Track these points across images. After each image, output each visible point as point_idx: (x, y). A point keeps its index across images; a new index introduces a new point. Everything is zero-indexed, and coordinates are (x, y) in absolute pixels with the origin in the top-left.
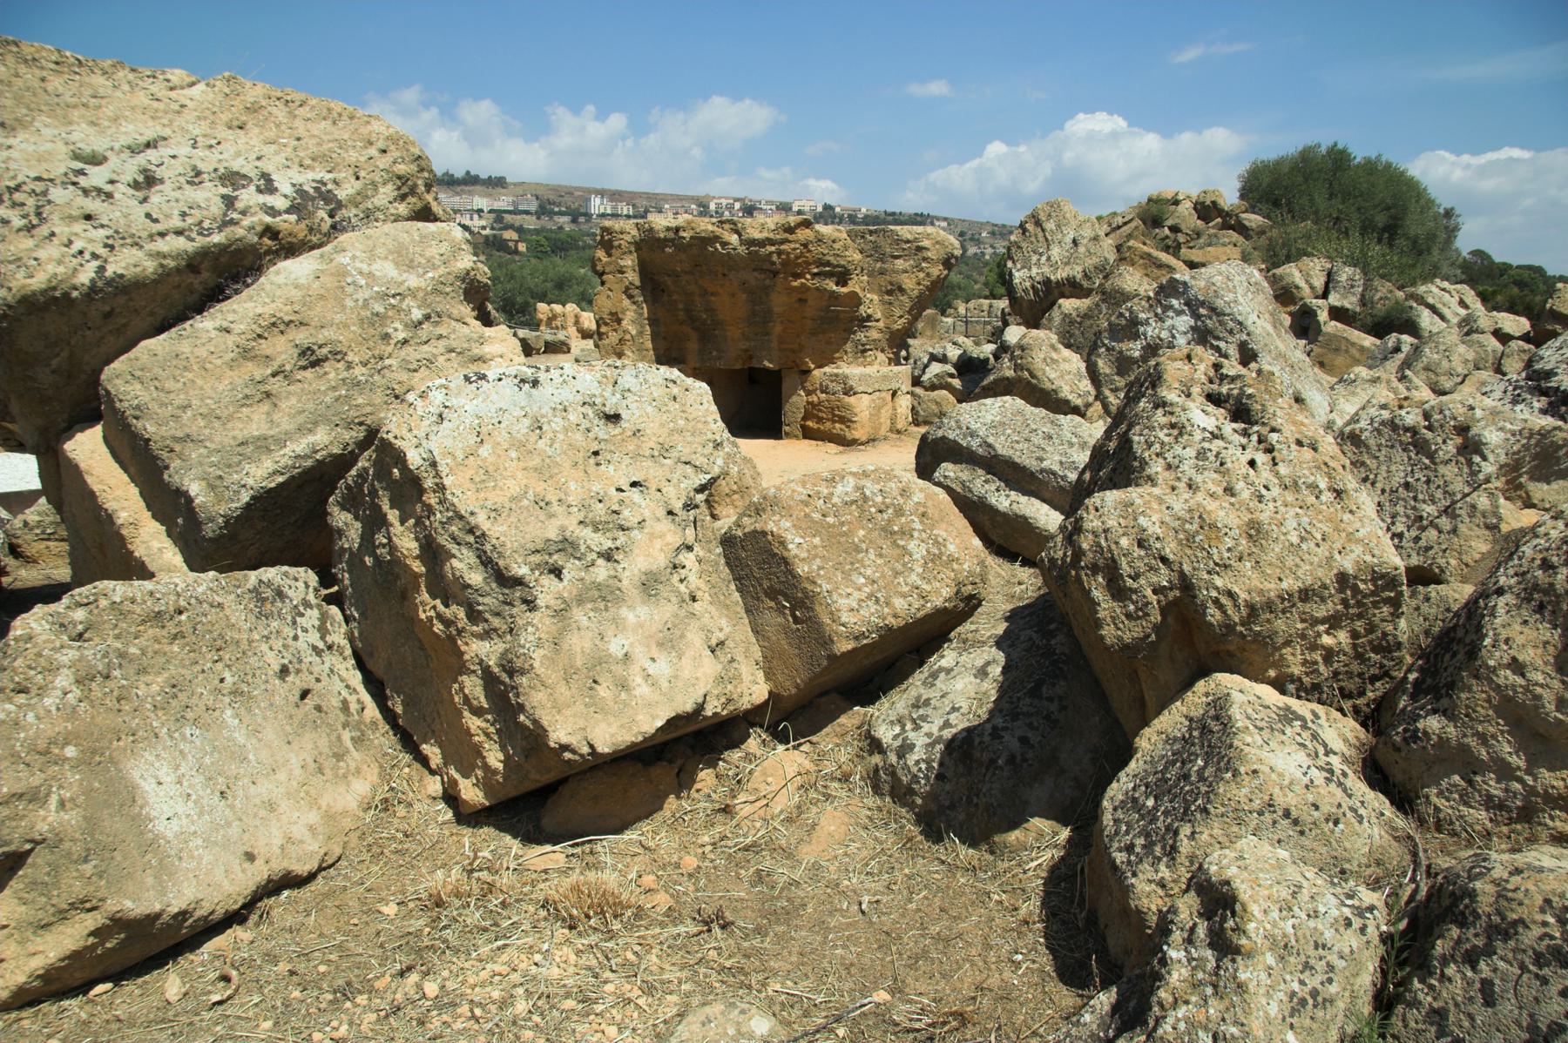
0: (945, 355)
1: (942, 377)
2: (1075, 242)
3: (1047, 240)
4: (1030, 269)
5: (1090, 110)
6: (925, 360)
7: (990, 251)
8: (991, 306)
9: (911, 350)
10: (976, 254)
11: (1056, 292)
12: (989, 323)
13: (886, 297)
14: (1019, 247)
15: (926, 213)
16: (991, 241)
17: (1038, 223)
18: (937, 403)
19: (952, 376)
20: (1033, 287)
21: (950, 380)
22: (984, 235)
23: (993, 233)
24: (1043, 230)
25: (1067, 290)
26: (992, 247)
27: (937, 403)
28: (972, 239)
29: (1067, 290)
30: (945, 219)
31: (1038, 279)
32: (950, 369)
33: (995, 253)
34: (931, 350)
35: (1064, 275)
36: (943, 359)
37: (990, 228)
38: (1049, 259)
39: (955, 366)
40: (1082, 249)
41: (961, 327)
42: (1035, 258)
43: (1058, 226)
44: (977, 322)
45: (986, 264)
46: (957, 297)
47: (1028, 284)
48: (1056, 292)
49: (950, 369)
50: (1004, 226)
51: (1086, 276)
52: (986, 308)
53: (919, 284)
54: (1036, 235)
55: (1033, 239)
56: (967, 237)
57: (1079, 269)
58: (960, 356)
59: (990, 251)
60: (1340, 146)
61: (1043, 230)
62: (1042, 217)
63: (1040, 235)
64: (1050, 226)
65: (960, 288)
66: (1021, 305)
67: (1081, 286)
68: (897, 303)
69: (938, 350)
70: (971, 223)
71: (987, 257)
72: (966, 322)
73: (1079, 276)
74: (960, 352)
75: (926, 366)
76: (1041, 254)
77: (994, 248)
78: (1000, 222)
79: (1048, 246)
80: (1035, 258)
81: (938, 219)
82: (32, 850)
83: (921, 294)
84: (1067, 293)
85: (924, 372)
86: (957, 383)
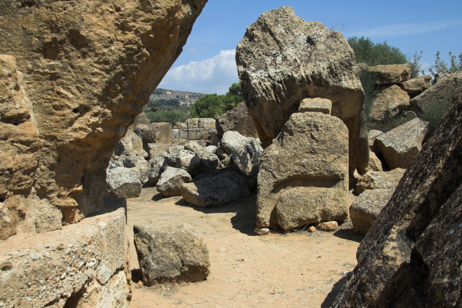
0: (178, 160)
1: (177, 181)
2: (310, 41)
3: (278, 42)
4: (266, 69)
5: (225, 49)
6: (161, 163)
7: (189, 103)
8: (199, 122)
9: (151, 151)
10: (184, 105)
11: (300, 91)
12: (199, 131)
13: (44, 62)
14: (248, 52)
15: (162, 88)
16: (189, 99)
17: (266, 28)
18: (177, 248)
19: (186, 180)
20: (274, 87)
21: (185, 185)
22: (186, 97)
23: (190, 96)
24: (272, 34)
25: (311, 88)
26: (190, 101)
27: (177, 248)
28: (181, 99)
29: (311, 88)
30: (170, 91)
31: (278, 78)
32: (184, 173)
33: (191, 104)
34: (166, 154)
35: (309, 72)
36: (176, 163)
37: (189, 94)
38: (285, 58)
39: (190, 169)
40: (321, 47)
41: (184, 134)
42: (269, 60)
43: (288, 30)
44: (192, 131)
45: (188, 109)
46: (178, 120)
47: (268, 84)
48: (300, 91)
49: (184, 173)
50: (194, 93)
51: (332, 72)
52: (196, 123)
53: (123, 27)
54: (266, 41)
55: (263, 43)
56: (180, 98)
57: (324, 65)
58: (193, 160)
59: (189, 103)
60: (365, 39)
61: (272, 34)
62: (269, 22)
63: (270, 39)
64: (279, 30)
65: (179, 116)
66: (261, 106)
67: (327, 83)
68: (70, 75)
69: (172, 155)
70: (181, 92)
71: (188, 106)
72: (188, 131)
73: (325, 73)
74: (192, 156)
75: (162, 170)
76: (275, 56)
77: (191, 102)
78: (192, 92)
79: (281, 49)
80: (269, 60)
81: (168, 91)
82: (115, 167)
83: (130, 53)
84: (311, 92)
85: (159, 177)
86: (192, 187)
